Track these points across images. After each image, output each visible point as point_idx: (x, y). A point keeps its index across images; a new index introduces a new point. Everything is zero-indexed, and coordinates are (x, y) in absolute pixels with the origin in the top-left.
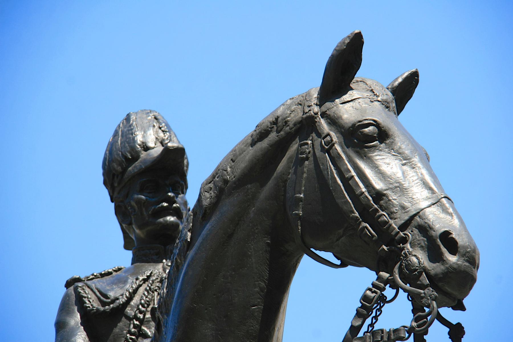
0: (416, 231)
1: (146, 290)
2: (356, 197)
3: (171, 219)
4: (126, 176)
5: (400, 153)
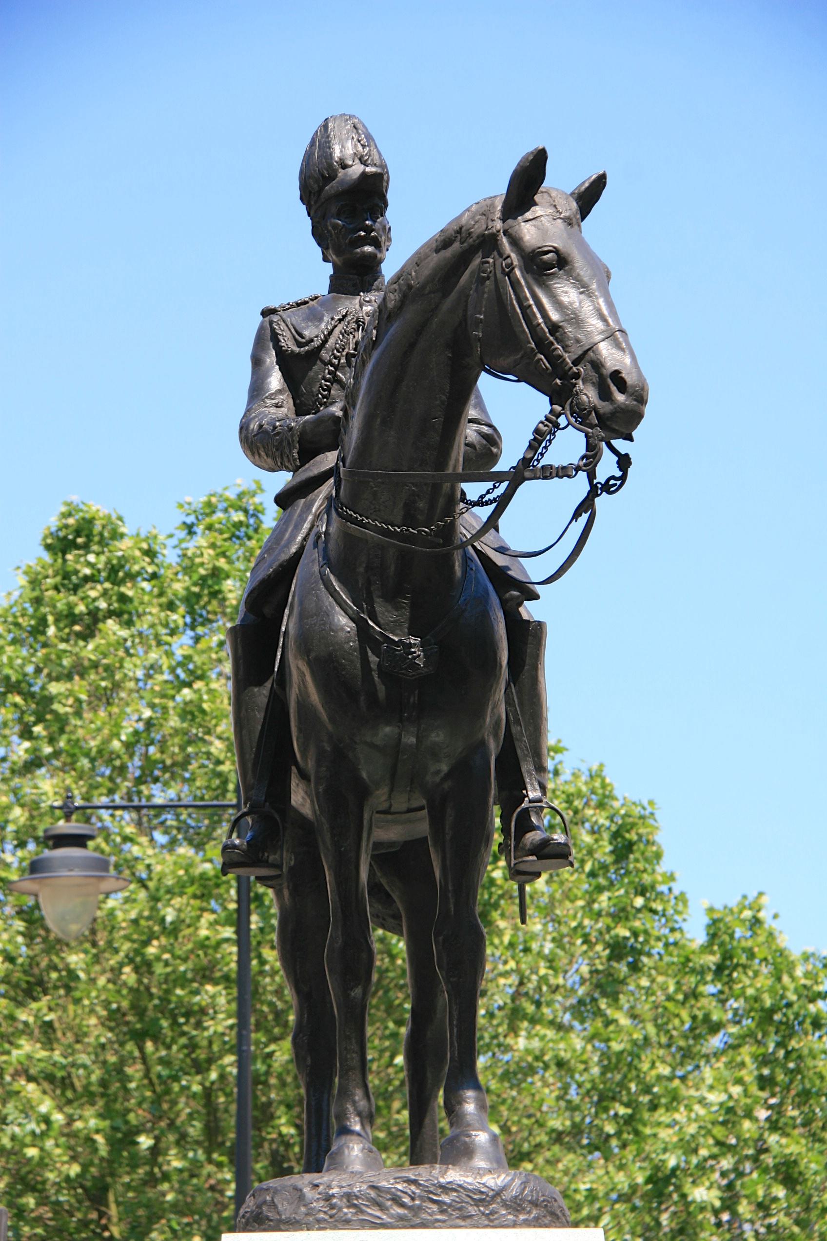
0: (589, 366)
2: (533, 327)
3: (368, 249)
4: (323, 195)
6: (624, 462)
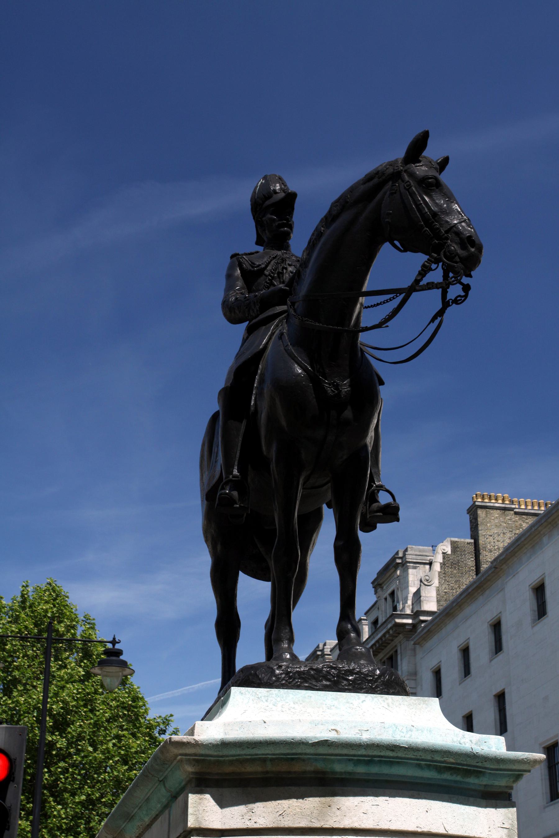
0: (453, 235)
1: (275, 262)
2: (423, 215)
5: (445, 195)
6: (467, 288)
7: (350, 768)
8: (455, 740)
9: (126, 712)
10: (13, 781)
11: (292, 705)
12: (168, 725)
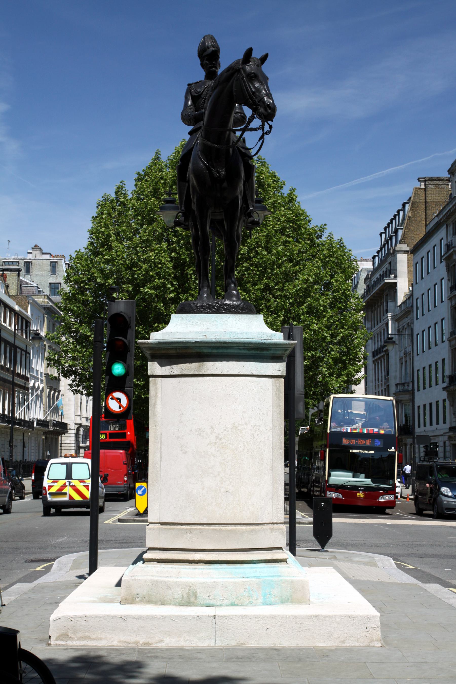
2: (249, 93)
6: (271, 127)
7: (210, 351)
8: (259, 336)
9: (291, 225)
10: (130, 328)
11: (197, 321)
12: (323, 231)
